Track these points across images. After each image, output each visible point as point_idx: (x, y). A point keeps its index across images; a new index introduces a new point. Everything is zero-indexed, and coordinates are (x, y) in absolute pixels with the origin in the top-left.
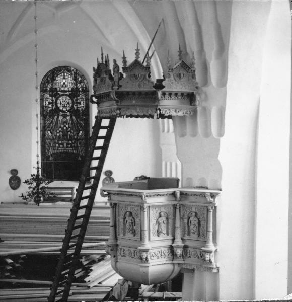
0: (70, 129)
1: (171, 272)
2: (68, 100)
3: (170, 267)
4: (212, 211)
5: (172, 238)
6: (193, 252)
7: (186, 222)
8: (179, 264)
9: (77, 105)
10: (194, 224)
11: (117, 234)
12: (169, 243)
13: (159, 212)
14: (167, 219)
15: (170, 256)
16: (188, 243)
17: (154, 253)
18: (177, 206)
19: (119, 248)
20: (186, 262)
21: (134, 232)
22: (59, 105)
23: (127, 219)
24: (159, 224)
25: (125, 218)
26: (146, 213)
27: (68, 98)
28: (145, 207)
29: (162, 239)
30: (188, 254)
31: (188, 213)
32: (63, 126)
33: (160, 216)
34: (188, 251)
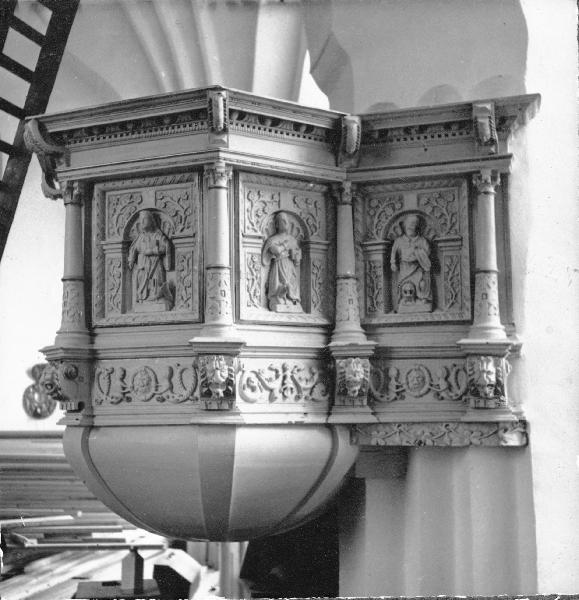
1: (323, 465)
3: (318, 441)
4: (492, 189)
6: (414, 374)
7: (378, 258)
8: (352, 428)
10: (416, 262)
11: (95, 310)
12: (316, 341)
13: (272, 208)
14: (304, 245)
15: (317, 394)
16: (388, 339)
17: (258, 375)
18: (341, 190)
19: (103, 367)
20: (383, 419)
21: (169, 295)
23: (136, 245)
24: (273, 261)
25: (127, 244)
26: (223, 194)
28: (222, 167)
29: (284, 319)
30: (393, 383)
31: (385, 223)
33: (277, 228)
34: (393, 373)
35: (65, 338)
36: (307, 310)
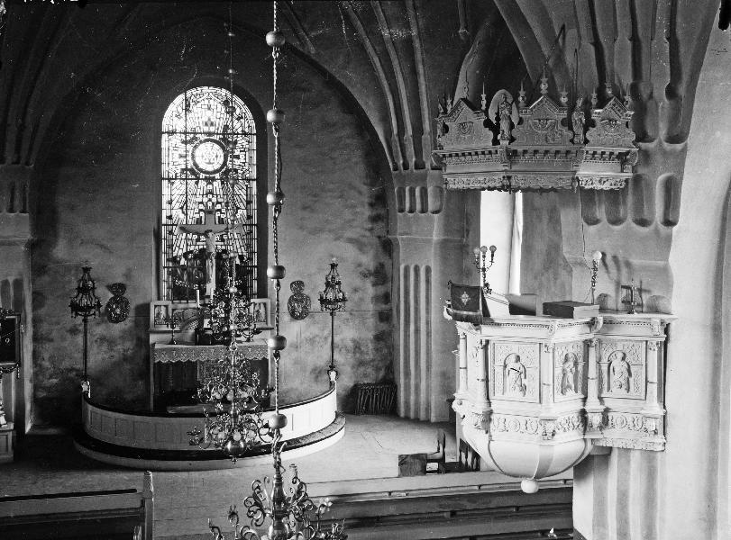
0: (219, 207)
2: (217, 150)
3: (582, 444)
5: (583, 396)
9: (232, 161)
12: (579, 406)
14: (576, 364)
16: (608, 403)
22: (198, 161)
27: (216, 146)
32: (205, 200)
34: (610, 418)
35: (600, 200)
36: (576, 392)
